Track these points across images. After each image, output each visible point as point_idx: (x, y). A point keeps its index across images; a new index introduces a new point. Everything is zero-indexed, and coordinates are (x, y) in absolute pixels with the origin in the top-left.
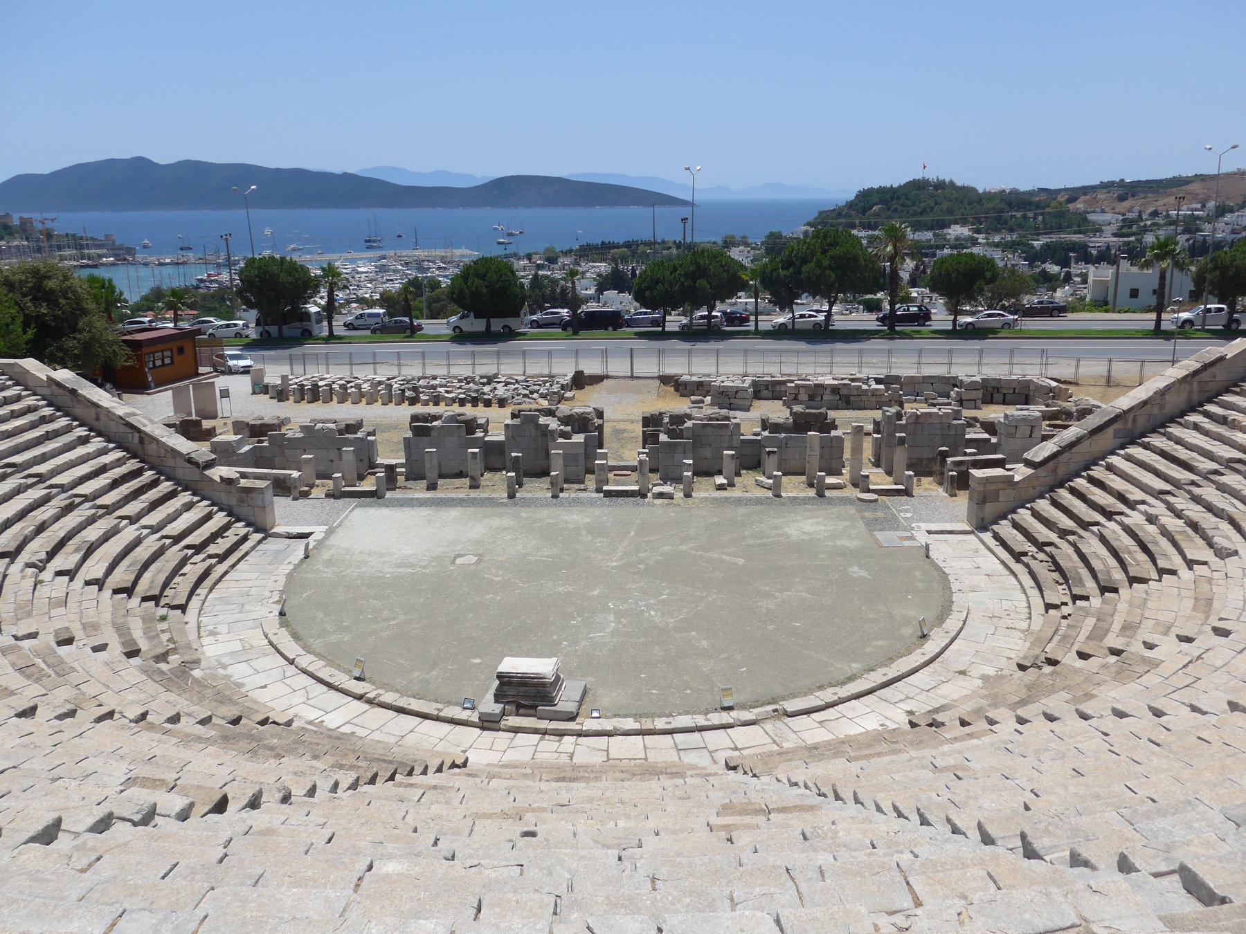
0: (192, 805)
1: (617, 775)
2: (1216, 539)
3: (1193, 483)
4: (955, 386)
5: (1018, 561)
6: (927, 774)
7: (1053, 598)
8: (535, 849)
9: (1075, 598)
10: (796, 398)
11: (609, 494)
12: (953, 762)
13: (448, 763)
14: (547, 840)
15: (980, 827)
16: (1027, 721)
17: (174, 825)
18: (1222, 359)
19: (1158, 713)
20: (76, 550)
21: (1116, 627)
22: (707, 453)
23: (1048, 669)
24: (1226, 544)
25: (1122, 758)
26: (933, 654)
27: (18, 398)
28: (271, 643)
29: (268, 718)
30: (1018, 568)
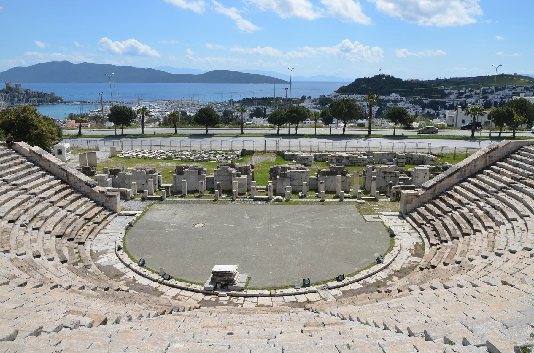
0: (93, 322)
1: (262, 312)
2: (496, 218)
3: (487, 196)
4: (395, 157)
5: (420, 227)
6: (386, 310)
7: (433, 241)
8: (233, 339)
9: (442, 241)
10: (331, 161)
11: (256, 199)
12: (396, 306)
13: (193, 307)
14: (238, 336)
15: (409, 329)
16: (424, 290)
17: (86, 329)
18: (498, 148)
19: (475, 286)
20: (41, 220)
21: (458, 252)
22: (296, 183)
23: (431, 269)
24: (500, 220)
25: (462, 303)
26: (387, 264)
27: (18, 158)
28: (119, 259)
29: (119, 289)
30: (420, 230)
